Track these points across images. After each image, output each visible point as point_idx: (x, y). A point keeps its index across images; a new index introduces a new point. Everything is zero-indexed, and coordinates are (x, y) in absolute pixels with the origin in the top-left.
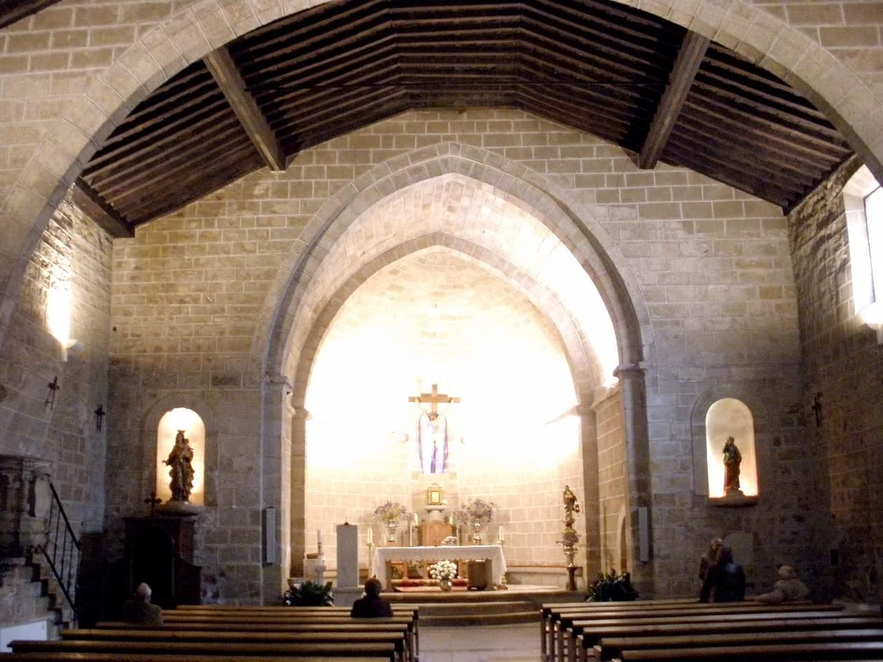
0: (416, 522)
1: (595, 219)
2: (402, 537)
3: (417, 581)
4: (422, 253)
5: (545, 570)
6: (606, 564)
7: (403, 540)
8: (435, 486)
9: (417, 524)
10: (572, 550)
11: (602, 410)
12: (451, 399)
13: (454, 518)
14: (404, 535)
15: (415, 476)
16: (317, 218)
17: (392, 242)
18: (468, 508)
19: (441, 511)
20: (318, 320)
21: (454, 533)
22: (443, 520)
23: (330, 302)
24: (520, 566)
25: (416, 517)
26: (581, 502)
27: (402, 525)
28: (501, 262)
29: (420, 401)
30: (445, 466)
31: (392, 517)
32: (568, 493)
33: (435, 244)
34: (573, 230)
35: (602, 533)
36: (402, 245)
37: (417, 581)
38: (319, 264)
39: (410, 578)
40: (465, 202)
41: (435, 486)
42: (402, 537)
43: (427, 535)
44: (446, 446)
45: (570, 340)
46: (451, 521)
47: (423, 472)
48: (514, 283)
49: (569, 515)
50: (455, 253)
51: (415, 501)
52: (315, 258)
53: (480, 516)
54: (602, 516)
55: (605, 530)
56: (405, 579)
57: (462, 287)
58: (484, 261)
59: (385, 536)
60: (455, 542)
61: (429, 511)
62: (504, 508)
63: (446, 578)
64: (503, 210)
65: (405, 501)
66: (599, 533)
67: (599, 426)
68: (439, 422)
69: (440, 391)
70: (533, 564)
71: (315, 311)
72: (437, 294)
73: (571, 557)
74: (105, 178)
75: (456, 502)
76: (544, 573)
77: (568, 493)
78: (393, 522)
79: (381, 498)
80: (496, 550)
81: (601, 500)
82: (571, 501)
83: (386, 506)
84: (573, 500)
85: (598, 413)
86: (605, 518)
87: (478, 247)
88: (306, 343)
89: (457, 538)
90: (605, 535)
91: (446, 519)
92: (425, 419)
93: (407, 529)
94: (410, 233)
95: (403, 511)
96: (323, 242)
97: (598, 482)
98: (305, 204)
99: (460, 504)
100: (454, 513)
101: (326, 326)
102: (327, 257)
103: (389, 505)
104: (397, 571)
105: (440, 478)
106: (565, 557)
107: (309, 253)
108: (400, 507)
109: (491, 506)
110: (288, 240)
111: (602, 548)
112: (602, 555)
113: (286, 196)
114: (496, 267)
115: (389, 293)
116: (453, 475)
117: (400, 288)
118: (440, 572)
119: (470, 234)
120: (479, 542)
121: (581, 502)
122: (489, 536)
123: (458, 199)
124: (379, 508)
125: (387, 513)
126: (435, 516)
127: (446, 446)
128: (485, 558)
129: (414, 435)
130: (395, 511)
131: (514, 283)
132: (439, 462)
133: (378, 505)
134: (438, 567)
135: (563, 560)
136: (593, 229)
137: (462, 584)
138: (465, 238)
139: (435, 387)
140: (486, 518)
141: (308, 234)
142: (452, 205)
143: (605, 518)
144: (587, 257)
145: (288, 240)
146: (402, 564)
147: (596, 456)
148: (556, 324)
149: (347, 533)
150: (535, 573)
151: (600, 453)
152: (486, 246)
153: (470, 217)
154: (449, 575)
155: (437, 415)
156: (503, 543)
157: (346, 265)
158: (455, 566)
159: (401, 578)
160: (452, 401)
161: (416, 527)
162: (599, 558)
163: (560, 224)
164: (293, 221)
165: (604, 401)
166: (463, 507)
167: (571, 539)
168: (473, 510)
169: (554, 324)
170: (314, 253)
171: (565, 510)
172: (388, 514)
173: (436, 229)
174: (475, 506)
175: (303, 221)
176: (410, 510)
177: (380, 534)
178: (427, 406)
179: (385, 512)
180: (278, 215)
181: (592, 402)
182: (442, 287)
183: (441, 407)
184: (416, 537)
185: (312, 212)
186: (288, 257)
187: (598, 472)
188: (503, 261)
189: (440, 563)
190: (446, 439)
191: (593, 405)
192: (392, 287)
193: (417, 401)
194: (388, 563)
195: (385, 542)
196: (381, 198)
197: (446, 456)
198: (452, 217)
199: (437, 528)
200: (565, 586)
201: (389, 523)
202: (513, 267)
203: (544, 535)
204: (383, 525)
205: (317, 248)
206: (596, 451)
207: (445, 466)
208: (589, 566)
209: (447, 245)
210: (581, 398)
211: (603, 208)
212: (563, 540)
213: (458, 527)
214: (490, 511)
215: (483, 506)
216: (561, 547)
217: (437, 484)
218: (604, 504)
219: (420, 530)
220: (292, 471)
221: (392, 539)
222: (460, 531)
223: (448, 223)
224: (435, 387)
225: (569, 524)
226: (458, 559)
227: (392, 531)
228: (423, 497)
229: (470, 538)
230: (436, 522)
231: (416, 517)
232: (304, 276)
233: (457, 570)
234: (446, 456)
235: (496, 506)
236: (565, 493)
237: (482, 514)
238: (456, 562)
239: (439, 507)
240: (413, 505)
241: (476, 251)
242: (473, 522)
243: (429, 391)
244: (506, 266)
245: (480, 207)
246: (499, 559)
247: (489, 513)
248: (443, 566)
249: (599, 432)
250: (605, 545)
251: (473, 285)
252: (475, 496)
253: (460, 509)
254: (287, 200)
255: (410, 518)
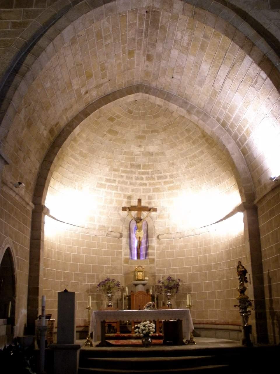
0: (127, 292)
1: (270, 20)
2: (117, 303)
3: (126, 335)
4: (131, 98)
5: (219, 327)
6: (273, 324)
7: (118, 305)
8: (140, 268)
9: (128, 294)
10: (246, 312)
11: (264, 203)
12: (151, 208)
13: (153, 290)
14: (119, 301)
15: (126, 261)
16: (37, 23)
17: (108, 89)
18: (163, 283)
19: (144, 285)
20: (54, 142)
21: (153, 300)
22: (145, 292)
23: (63, 129)
24: (200, 324)
25: (127, 289)
26: (249, 275)
27: (117, 295)
28: (185, 103)
29: (130, 210)
30: (147, 254)
31: (110, 289)
32: (240, 267)
33: (138, 92)
34: (251, 32)
35: (267, 298)
36: (115, 92)
37: (126, 335)
38: (36, 59)
39: (121, 332)
40: (159, 48)
41: (140, 268)
42: (117, 303)
43: (134, 303)
44: (147, 242)
45: (236, 155)
46: (151, 292)
47: (132, 259)
48: (195, 118)
49: (242, 285)
50: (153, 97)
51: (127, 279)
52: (33, 54)
53: (171, 288)
54: (266, 285)
55: (271, 296)
56: (119, 334)
57: (157, 131)
58: (172, 103)
59: (105, 302)
60: (154, 306)
61: (136, 285)
62: (187, 282)
63: (147, 335)
64: (187, 49)
65: (119, 277)
66: (264, 298)
67: (260, 217)
68: (142, 224)
69: (143, 204)
70: (209, 322)
71: (51, 131)
72: (140, 137)
73: (246, 318)
74: (136, 298)
75: (154, 279)
76: (217, 329)
77: (240, 267)
78: (111, 293)
79: (103, 276)
80: (185, 313)
81: (266, 272)
82: (242, 274)
83: (106, 281)
84: (245, 272)
85: (260, 207)
86: (270, 287)
87: (168, 94)
88: (45, 158)
89: (155, 303)
90: (271, 301)
91: (148, 291)
92: (134, 225)
93: (121, 298)
94: (121, 82)
95: (118, 285)
96: (41, 42)
97: (261, 260)
98: (27, 12)
99: (157, 281)
100: (153, 287)
101: (60, 146)
102: (43, 54)
103: (108, 280)
104: (113, 327)
105: (144, 263)
106: (241, 318)
107: (29, 51)
108: (116, 282)
109: (178, 281)
110: (9, 38)
111: (268, 311)
112: (268, 315)
113: (11, 7)
114: (182, 107)
115: (109, 135)
116: (153, 261)
117: (116, 133)
118: (143, 330)
119: (163, 82)
120: (170, 306)
121: (249, 275)
122: (176, 303)
123: (154, 45)
124: (101, 282)
125: (107, 286)
126: (140, 288)
127: (147, 242)
128: (177, 319)
129: (125, 233)
130: (112, 285)
131: (195, 118)
132: (143, 252)
133: (101, 281)
134: (141, 326)
135: (240, 321)
136: (269, 28)
137: (159, 338)
138: (160, 87)
139: (140, 201)
140: (175, 290)
141: (27, 34)
142: (150, 53)
143: (270, 287)
144: (265, 52)
145: (9, 38)
146: (116, 322)
147: (259, 239)
148: (226, 145)
149: (66, 299)
150: (212, 329)
151: (262, 237)
152: (174, 92)
153: (163, 63)
154: (149, 333)
155: (141, 220)
156: (190, 307)
157: (73, 100)
158: (154, 326)
159: (115, 333)
160: (151, 210)
161: (127, 296)
162: (265, 318)
163: (239, 28)
164: (15, 25)
165: (268, 194)
166: (159, 282)
167: (244, 303)
168: (166, 284)
169: (224, 145)
170: (32, 51)
171: (239, 281)
172: (107, 287)
173: (140, 81)
174: (167, 281)
175: (23, 25)
176: (122, 284)
177: (102, 301)
178: (134, 213)
179: (105, 285)
180: (4, 21)
181: (254, 199)
182: (144, 132)
183: (145, 214)
184: (127, 304)
185: (33, 18)
186: (9, 51)
187: (261, 251)
188: (186, 103)
189: (142, 324)
190: (147, 237)
191: (256, 202)
192: (111, 131)
193: (128, 210)
194: (103, 323)
195: (105, 306)
196: (91, 10)
197: (147, 248)
198: (152, 68)
199: (141, 296)
200: (241, 342)
201: (108, 293)
202: (193, 107)
203: (216, 301)
204: (104, 295)
205: (35, 47)
206: (259, 236)
207: (147, 254)
208: (257, 325)
209: (147, 93)
210: (246, 197)
211: (276, 13)
212: (238, 304)
213: (156, 296)
214: (178, 285)
215: (173, 281)
216: (237, 309)
217: (141, 267)
218: (268, 276)
219: (129, 298)
220: (31, 251)
221: (110, 304)
222: (157, 299)
223: (147, 74)
224: (140, 201)
225: (243, 291)
226: (156, 320)
227: (110, 299)
228: (132, 275)
229: (164, 304)
230: (140, 292)
231: (127, 289)
232: (23, 68)
233: (155, 329)
234: (147, 248)
235: (182, 281)
236: (238, 267)
237: (172, 286)
238: (155, 322)
239: (143, 282)
240: (125, 282)
241: (167, 96)
242: (166, 292)
243: (135, 203)
244: (189, 106)
245: (170, 50)
246: (188, 319)
247: (177, 286)
248: (144, 326)
249: (260, 221)
250: (271, 308)
251: (164, 130)
252: (167, 275)
253: (157, 284)
254: (12, 10)
255: (123, 290)
